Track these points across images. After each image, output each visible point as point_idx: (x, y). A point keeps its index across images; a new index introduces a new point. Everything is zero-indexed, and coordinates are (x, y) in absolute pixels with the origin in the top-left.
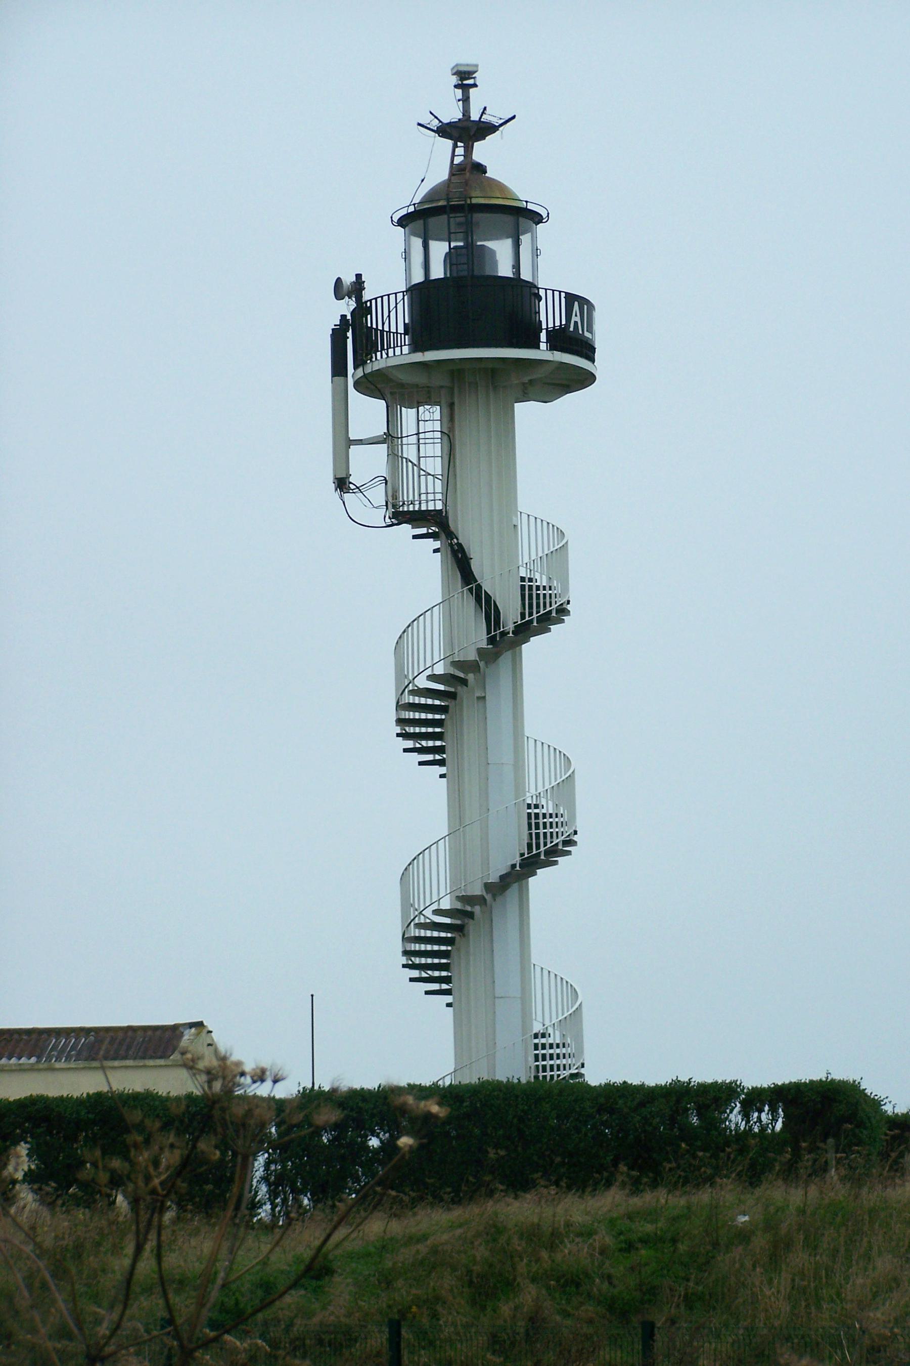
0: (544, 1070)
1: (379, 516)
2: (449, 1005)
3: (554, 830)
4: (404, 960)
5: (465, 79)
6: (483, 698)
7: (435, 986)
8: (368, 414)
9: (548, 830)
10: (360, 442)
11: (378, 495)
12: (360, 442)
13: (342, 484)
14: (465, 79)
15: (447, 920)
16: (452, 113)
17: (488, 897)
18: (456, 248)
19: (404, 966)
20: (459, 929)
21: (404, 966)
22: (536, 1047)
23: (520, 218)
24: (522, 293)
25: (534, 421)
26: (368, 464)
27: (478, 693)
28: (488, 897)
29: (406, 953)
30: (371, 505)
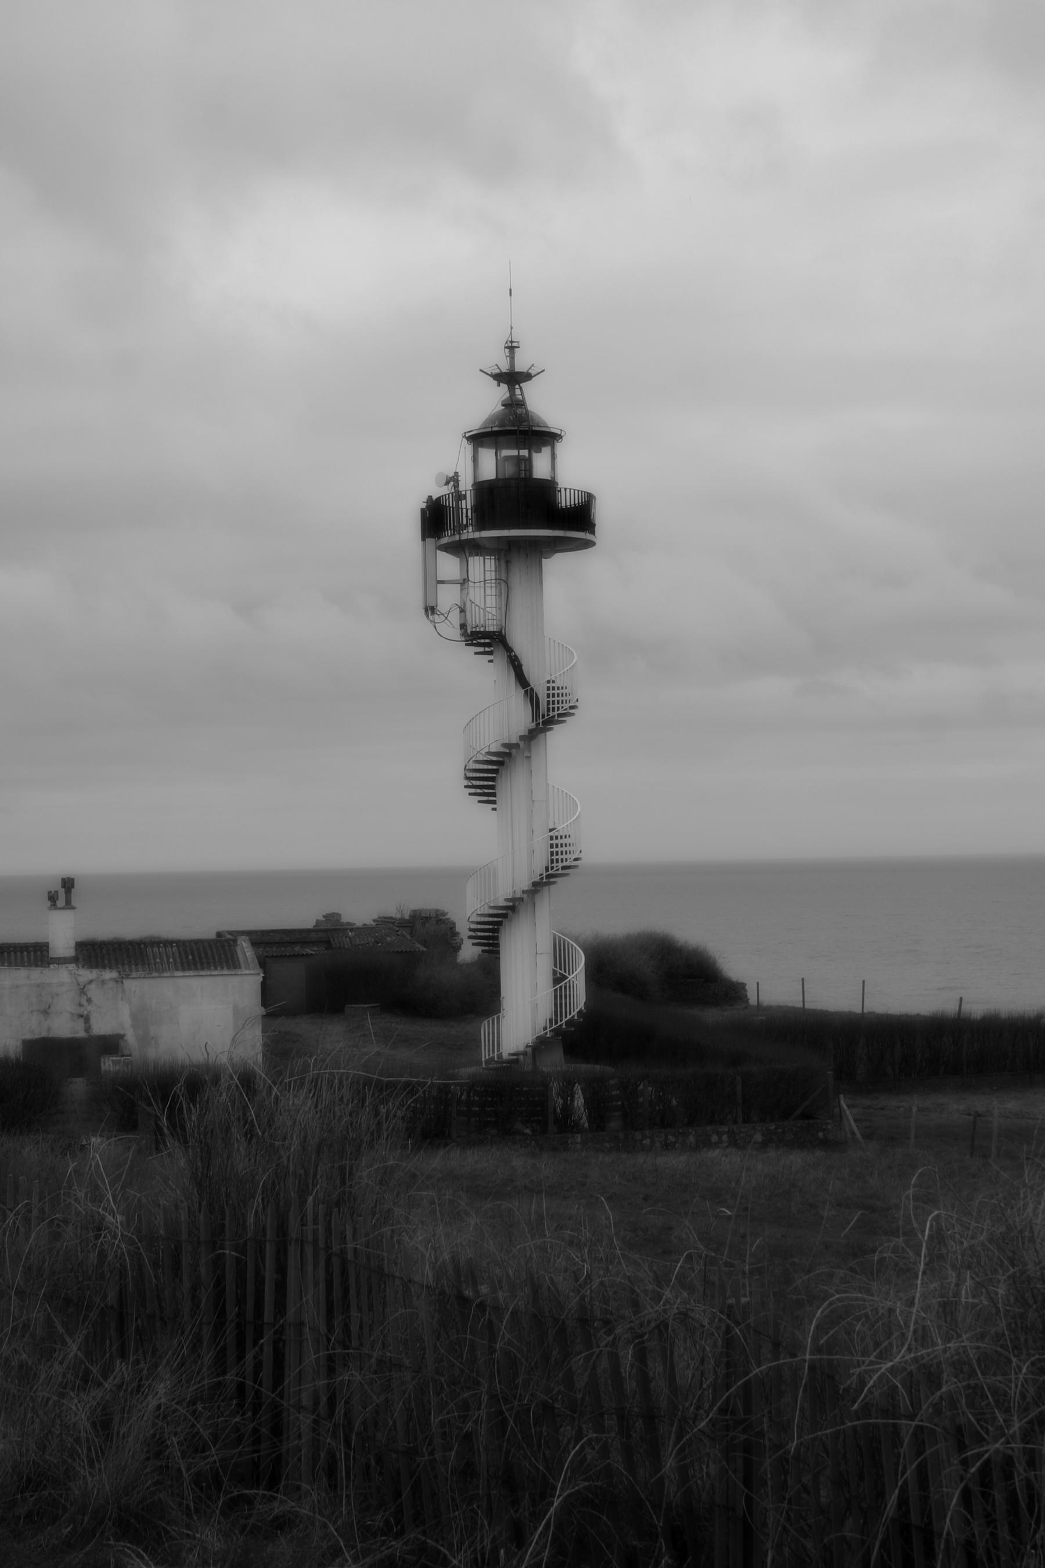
0: (557, 854)
1: (456, 633)
2: (491, 661)
3: (560, 698)
4: (466, 783)
5: (511, 348)
6: (529, 757)
7: (481, 649)
8: (448, 565)
9: (556, 699)
10: (442, 582)
11: (455, 618)
12: (442, 582)
13: (430, 610)
14: (511, 348)
15: (494, 758)
16: (505, 368)
17: (522, 744)
18: (507, 458)
19: (466, 787)
20: (501, 763)
21: (466, 787)
22: (551, 838)
23: (546, 438)
24: (548, 488)
25: (559, 568)
26: (448, 598)
27: (527, 754)
28: (522, 744)
29: (467, 778)
30: (451, 628)
